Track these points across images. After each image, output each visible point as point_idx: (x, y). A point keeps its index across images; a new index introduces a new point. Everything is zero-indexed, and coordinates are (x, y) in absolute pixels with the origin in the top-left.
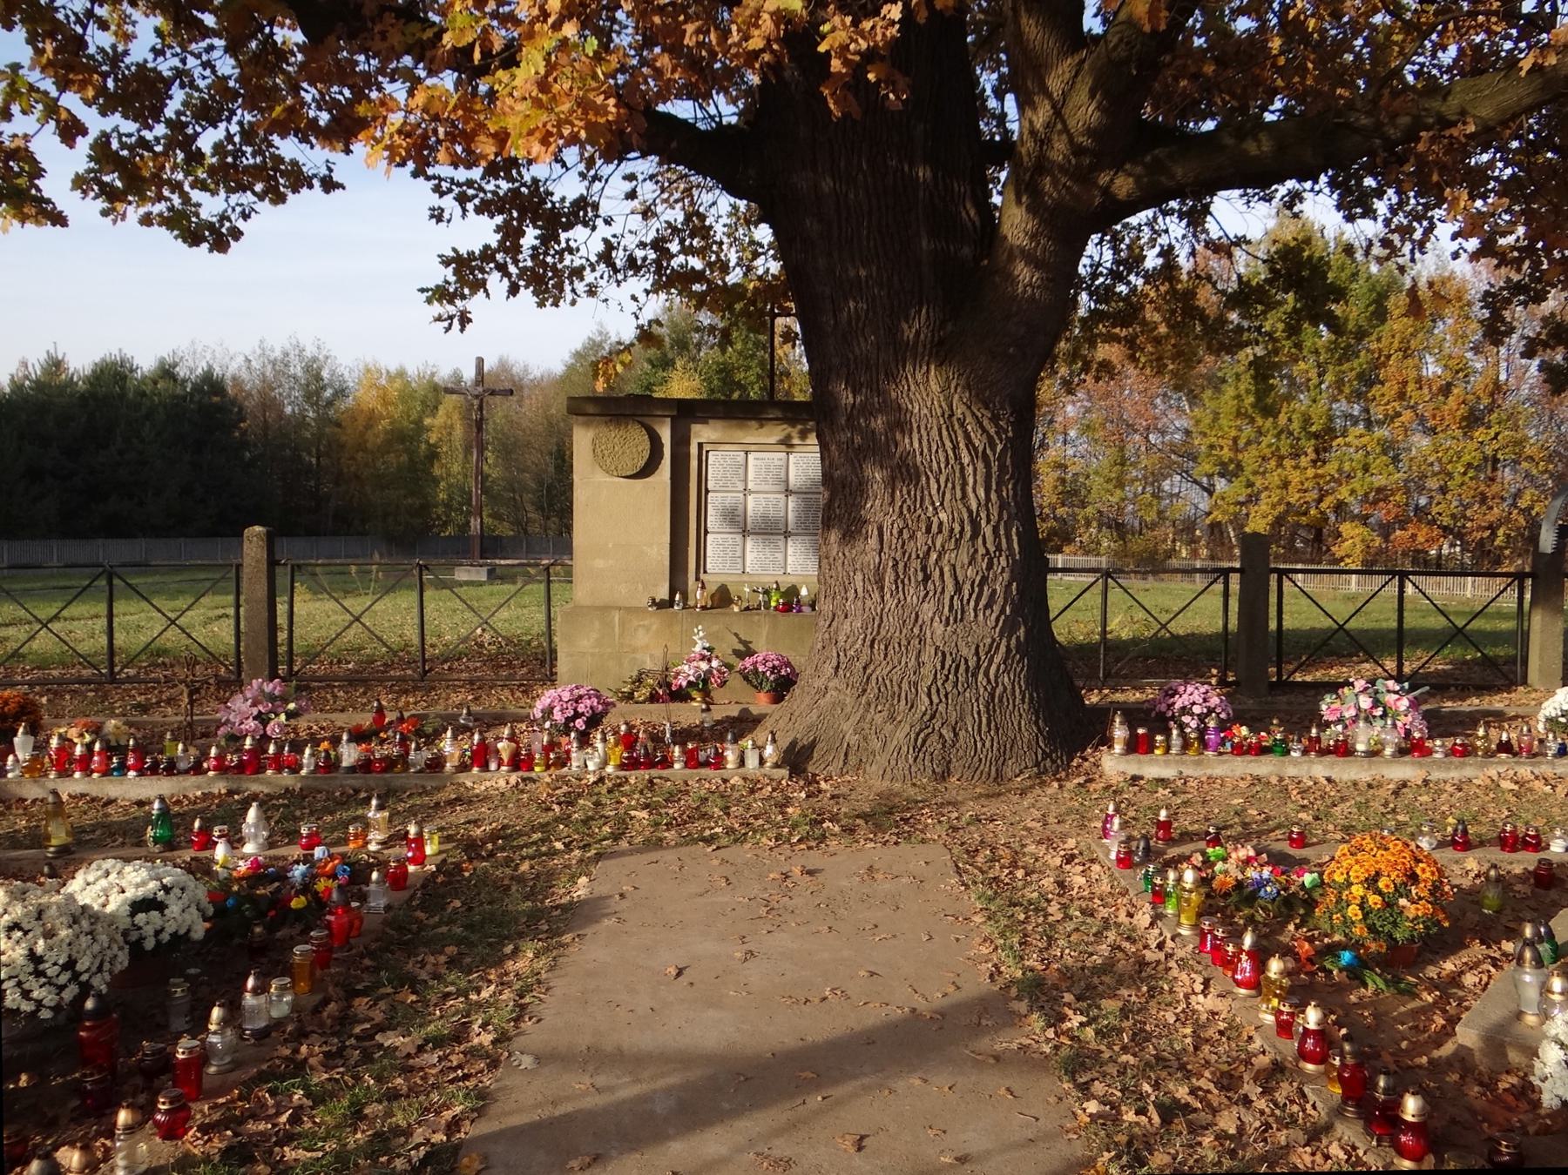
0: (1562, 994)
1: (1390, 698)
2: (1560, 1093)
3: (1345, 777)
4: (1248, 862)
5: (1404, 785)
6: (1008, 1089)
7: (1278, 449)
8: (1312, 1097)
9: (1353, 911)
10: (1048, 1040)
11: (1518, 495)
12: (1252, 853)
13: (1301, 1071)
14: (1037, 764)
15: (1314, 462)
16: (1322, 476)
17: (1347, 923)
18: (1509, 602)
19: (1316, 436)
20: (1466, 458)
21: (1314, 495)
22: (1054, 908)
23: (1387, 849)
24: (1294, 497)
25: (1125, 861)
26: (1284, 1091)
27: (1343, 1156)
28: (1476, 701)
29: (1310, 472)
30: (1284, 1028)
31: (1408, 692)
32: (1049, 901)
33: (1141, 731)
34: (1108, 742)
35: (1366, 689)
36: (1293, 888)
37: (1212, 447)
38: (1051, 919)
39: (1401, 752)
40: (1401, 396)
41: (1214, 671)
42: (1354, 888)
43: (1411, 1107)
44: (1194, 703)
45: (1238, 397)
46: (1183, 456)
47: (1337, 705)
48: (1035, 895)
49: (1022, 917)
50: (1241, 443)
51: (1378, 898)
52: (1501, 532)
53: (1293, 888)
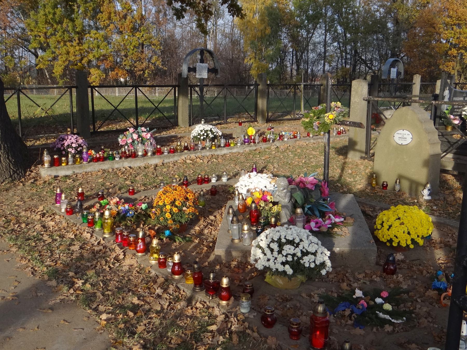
0: (247, 230)
1: (144, 134)
2: (264, 264)
3: (136, 166)
4: (117, 203)
5: (156, 166)
6: (64, 320)
7: (64, 37)
8: (182, 288)
9: (168, 215)
10: (72, 294)
11: (151, 58)
12: (118, 200)
13: (173, 279)
14: (11, 176)
15: (78, 44)
16: (82, 50)
17: (166, 220)
18: (171, 97)
19: (78, 33)
20: (134, 44)
21: (78, 58)
22: (46, 237)
23: (176, 190)
24: (72, 58)
25: (70, 211)
26: (171, 289)
27: (201, 306)
28: (165, 133)
29: (77, 48)
30: (162, 264)
31: (149, 132)
32: (42, 235)
33: (55, 157)
34: (42, 163)
35: (134, 131)
36: (139, 211)
37: (35, 36)
38: (47, 242)
39: (154, 153)
40: (109, 18)
41: (69, 129)
42: (167, 207)
43: (225, 281)
44: (72, 143)
45: (45, 15)
46: (23, 40)
47: (124, 139)
48: (35, 233)
49: (34, 244)
50: (49, 34)
51: (176, 209)
52: (146, 72)
53: (139, 211)
